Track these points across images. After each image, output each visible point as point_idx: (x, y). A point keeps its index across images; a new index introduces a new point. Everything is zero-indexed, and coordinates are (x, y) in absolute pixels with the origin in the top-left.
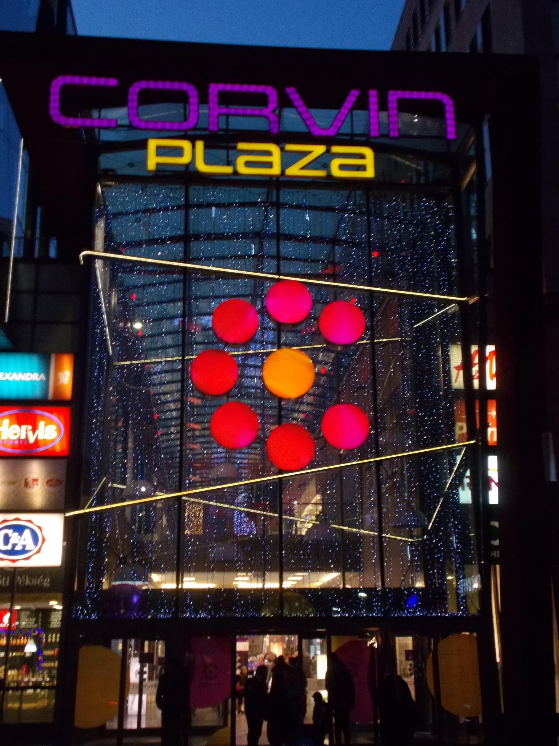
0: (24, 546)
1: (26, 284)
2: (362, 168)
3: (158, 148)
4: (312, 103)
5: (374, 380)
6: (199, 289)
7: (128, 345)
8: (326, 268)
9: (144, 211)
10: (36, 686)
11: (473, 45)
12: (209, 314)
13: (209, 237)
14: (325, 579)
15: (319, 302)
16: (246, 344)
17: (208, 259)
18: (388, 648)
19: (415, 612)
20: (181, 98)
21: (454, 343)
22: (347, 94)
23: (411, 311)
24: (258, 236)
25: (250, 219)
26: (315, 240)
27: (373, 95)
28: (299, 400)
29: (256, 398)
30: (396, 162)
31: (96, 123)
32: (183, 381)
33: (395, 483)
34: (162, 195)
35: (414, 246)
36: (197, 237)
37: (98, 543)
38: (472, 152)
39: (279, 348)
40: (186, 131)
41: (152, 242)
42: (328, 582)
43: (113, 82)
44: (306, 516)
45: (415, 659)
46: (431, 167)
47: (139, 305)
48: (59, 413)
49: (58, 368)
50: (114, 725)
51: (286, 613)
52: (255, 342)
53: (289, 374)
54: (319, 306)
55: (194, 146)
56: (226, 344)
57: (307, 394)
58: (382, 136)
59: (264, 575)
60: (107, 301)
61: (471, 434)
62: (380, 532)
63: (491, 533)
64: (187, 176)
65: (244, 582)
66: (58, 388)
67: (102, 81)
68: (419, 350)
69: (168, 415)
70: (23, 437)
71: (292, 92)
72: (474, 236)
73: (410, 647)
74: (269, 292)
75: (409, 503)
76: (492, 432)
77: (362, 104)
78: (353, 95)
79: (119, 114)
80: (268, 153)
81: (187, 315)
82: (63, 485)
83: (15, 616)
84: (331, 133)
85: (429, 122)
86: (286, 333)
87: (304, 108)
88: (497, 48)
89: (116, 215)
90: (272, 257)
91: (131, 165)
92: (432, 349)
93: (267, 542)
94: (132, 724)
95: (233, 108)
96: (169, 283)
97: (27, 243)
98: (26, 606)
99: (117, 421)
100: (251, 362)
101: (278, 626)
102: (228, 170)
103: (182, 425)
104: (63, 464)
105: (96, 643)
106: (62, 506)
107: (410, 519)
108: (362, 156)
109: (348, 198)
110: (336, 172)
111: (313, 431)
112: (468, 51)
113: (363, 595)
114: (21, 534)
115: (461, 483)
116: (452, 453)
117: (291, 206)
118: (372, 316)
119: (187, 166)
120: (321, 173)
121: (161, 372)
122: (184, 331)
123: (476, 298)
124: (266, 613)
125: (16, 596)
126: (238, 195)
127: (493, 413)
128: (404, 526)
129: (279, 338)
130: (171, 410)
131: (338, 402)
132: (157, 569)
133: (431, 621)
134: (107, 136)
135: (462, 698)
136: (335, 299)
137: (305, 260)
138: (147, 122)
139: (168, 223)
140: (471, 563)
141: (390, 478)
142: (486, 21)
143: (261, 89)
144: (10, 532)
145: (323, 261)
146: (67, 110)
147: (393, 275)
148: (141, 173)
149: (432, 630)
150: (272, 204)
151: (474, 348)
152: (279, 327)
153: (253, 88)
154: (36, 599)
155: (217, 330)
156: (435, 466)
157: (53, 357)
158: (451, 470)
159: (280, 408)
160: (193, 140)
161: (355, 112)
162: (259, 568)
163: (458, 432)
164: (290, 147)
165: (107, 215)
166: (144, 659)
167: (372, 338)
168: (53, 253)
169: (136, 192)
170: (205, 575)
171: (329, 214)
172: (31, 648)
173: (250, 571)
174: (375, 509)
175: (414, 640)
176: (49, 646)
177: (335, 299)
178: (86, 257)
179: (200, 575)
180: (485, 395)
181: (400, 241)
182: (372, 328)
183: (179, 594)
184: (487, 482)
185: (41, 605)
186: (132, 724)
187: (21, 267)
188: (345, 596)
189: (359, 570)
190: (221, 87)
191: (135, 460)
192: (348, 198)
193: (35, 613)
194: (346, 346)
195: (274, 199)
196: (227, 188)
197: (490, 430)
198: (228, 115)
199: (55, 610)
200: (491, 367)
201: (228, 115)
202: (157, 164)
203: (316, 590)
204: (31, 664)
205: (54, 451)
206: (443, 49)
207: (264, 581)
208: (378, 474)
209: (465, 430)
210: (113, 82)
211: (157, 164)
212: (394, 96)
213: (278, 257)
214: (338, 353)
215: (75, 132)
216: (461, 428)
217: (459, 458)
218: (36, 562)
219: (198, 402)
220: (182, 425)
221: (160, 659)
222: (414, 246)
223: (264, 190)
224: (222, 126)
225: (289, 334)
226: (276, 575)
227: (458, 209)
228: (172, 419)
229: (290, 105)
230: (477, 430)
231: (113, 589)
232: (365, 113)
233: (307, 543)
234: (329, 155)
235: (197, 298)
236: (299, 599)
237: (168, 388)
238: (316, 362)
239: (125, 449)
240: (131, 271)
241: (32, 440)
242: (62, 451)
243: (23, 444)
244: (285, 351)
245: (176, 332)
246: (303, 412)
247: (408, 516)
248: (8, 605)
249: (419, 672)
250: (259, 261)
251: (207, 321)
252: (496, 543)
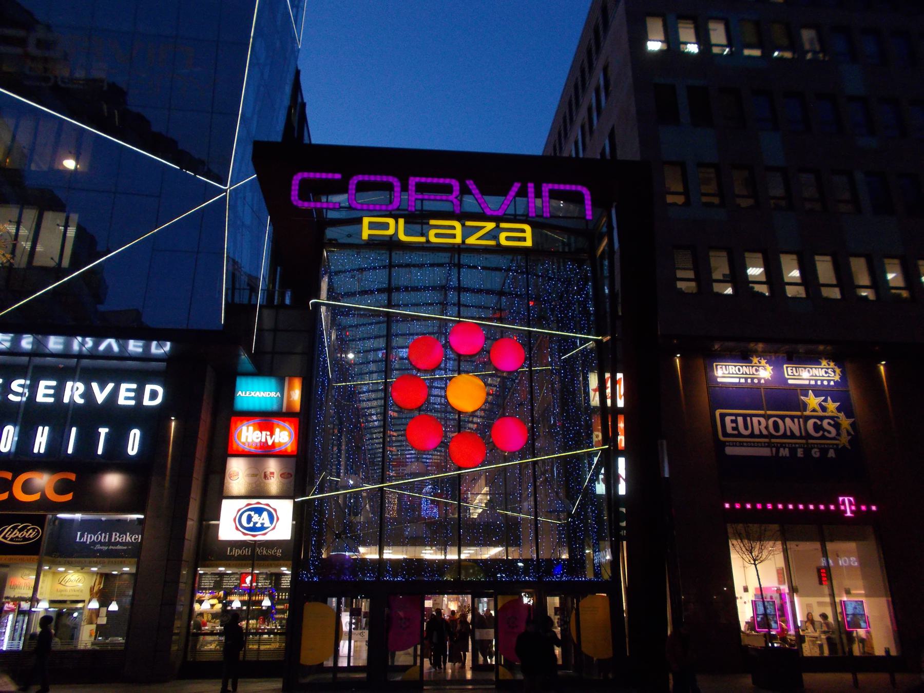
0: (262, 524)
1: (268, 324)
2: (524, 239)
3: (370, 223)
4: (485, 192)
5: (532, 399)
6: (396, 328)
7: (344, 370)
8: (495, 313)
9: (358, 270)
10: (270, 632)
11: (603, 153)
12: (406, 347)
13: (406, 289)
14: (492, 552)
15: (489, 339)
16: (433, 371)
17: (406, 306)
18: (541, 605)
19: (562, 577)
20: (389, 187)
21: (592, 371)
22: (512, 185)
23: (559, 347)
24: (444, 288)
25: (436, 276)
26: (488, 292)
27: (531, 187)
28: (473, 414)
29: (441, 412)
30: (547, 234)
31: (325, 206)
32: (385, 399)
33: (547, 478)
34: (372, 258)
35: (561, 298)
36: (398, 289)
37: (319, 522)
38: (605, 229)
39: (459, 374)
40: (391, 211)
41: (364, 293)
42: (495, 555)
43: (338, 176)
44: (478, 504)
45: (562, 614)
46: (573, 239)
47: (353, 340)
48: (290, 423)
49: (291, 388)
50: (330, 663)
51: (463, 577)
52: (441, 369)
53: (467, 393)
54: (489, 342)
55: (397, 222)
56: (419, 370)
57: (480, 409)
58: (537, 216)
59: (445, 549)
60: (330, 336)
61: (605, 440)
62: (536, 516)
63: (619, 517)
64: (392, 244)
65: (430, 554)
66: (290, 403)
67: (330, 176)
68: (565, 377)
69: (371, 425)
70: (263, 440)
71: (470, 183)
72: (607, 291)
73: (558, 605)
74: (451, 331)
75: (557, 493)
76: (621, 439)
77: (522, 193)
78: (516, 186)
79: (341, 199)
80: (453, 228)
81: (389, 348)
82: (293, 479)
83: (255, 578)
84: (500, 213)
85: (572, 207)
86: (463, 364)
87: (480, 195)
88: (621, 155)
89: (337, 273)
90: (454, 304)
91: (349, 236)
92: (574, 376)
93: (449, 523)
94: (343, 663)
95: (426, 195)
96: (376, 323)
97: (270, 294)
98: (265, 571)
99: (334, 428)
100: (435, 384)
101: (456, 589)
102: (423, 239)
103: (384, 433)
104: (293, 460)
105: (316, 600)
106: (292, 494)
107: (558, 505)
108: (523, 231)
109: (512, 261)
110: (504, 242)
111: (483, 438)
112: (599, 157)
113: (520, 564)
114: (260, 515)
115: (597, 479)
116: (590, 455)
117: (469, 267)
118: (530, 350)
119: (391, 237)
120: (492, 243)
121: (368, 391)
122: (387, 360)
123: (609, 338)
124: (448, 578)
125: (256, 562)
126: (428, 258)
127: (621, 425)
128: (554, 511)
129: (459, 366)
130: (374, 421)
131: (503, 415)
132: (365, 544)
133: (574, 585)
134: (332, 215)
135: (595, 638)
136: (502, 337)
137: (480, 307)
138: (361, 204)
139: (377, 279)
140: (605, 540)
141: (543, 474)
142: (612, 137)
143: (447, 181)
144: (252, 513)
145: (493, 308)
146: (303, 196)
147: (545, 319)
148: (356, 241)
149: (573, 592)
150: (455, 265)
151: (607, 375)
152: (459, 358)
153: (441, 181)
154: (271, 566)
155: (413, 358)
156: (578, 465)
157: (287, 379)
158: (590, 468)
159: (459, 420)
160: (396, 219)
161: (517, 199)
162: (443, 545)
163: (595, 439)
164: (468, 223)
165: (330, 273)
166: (355, 613)
167: (530, 366)
168: (288, 301)
169: (353, 256)
170: (400, 548)
171: (498, 273)
172: (267, 603)
173: (435, 545)
174: (532, 498)
175: (560, 599)
176: (281, 602)
177: (502, 337)
178: (314, 304)
179: (396, 548)
180: (615, 410)
181: (550, 294)
182: (530, 359)
183: (381, 562)
184: (617, 477)
185: (274, 570)
186: (343, 663)
187: (266, 312)
188: (506, 565)
189: (519, 545)
190: (418, 179)
191: (348, 459)
192: (512, 261)
193: (270, 576)
194: (510, 373)
195: (456, 261)
196: (421, 253)
197: (619, 438)
198: (422, 200)
199: (285, 574)
200: (621, 389)
201: (422, 200)
202: (369, 235)
203: (486, 560)
204: (266, 615)
205: (286, 451)
206: (581, 155)
207: (445, 553)
208: (534, 471)
209: (600, 438)
210: (338, 176)
211: (369, 235)
212: (546, 188)
213: (459, 304)
214: (503, 378)
215: (309, 212)
216: (597, 436)
217: (596, 459)
218: (271, 536)
219: (396, 415)
220: (384, 433)
221: (365, 613)
222: (561, 298)
223: (449, 255)
224: (418, 207)
225: (466, 363)
226: (456, 549)
227: (594, 271)
228: (376, 427)
229: (469, 192)
230: (610, 438)
231: (330, 558)
232: (525, 199)
233: (479, 524)
234: (498, 230)
235: (397, 335)
236: (473, 567)
237: (375, 403)
238: (486, 384)
239: (340, 450)
240: (348, 315)
241: (270, 443)
242: (292, 451)
243: (264, 445)
244: (464, 376)
245: (380, 361)
246: (477, 423)
247: (557, 503)
248: (249, 570)
249: (564, 623)
250: (443, 306)
251: (404, 353)
252: (624, 524)
